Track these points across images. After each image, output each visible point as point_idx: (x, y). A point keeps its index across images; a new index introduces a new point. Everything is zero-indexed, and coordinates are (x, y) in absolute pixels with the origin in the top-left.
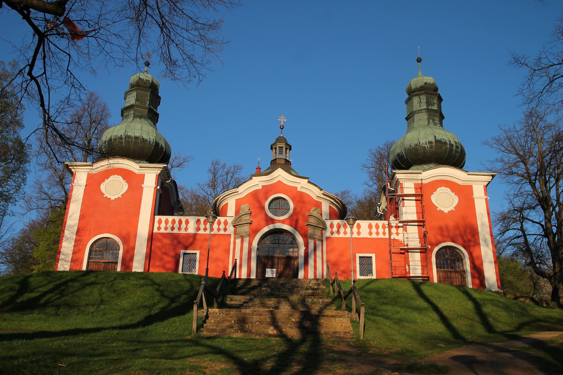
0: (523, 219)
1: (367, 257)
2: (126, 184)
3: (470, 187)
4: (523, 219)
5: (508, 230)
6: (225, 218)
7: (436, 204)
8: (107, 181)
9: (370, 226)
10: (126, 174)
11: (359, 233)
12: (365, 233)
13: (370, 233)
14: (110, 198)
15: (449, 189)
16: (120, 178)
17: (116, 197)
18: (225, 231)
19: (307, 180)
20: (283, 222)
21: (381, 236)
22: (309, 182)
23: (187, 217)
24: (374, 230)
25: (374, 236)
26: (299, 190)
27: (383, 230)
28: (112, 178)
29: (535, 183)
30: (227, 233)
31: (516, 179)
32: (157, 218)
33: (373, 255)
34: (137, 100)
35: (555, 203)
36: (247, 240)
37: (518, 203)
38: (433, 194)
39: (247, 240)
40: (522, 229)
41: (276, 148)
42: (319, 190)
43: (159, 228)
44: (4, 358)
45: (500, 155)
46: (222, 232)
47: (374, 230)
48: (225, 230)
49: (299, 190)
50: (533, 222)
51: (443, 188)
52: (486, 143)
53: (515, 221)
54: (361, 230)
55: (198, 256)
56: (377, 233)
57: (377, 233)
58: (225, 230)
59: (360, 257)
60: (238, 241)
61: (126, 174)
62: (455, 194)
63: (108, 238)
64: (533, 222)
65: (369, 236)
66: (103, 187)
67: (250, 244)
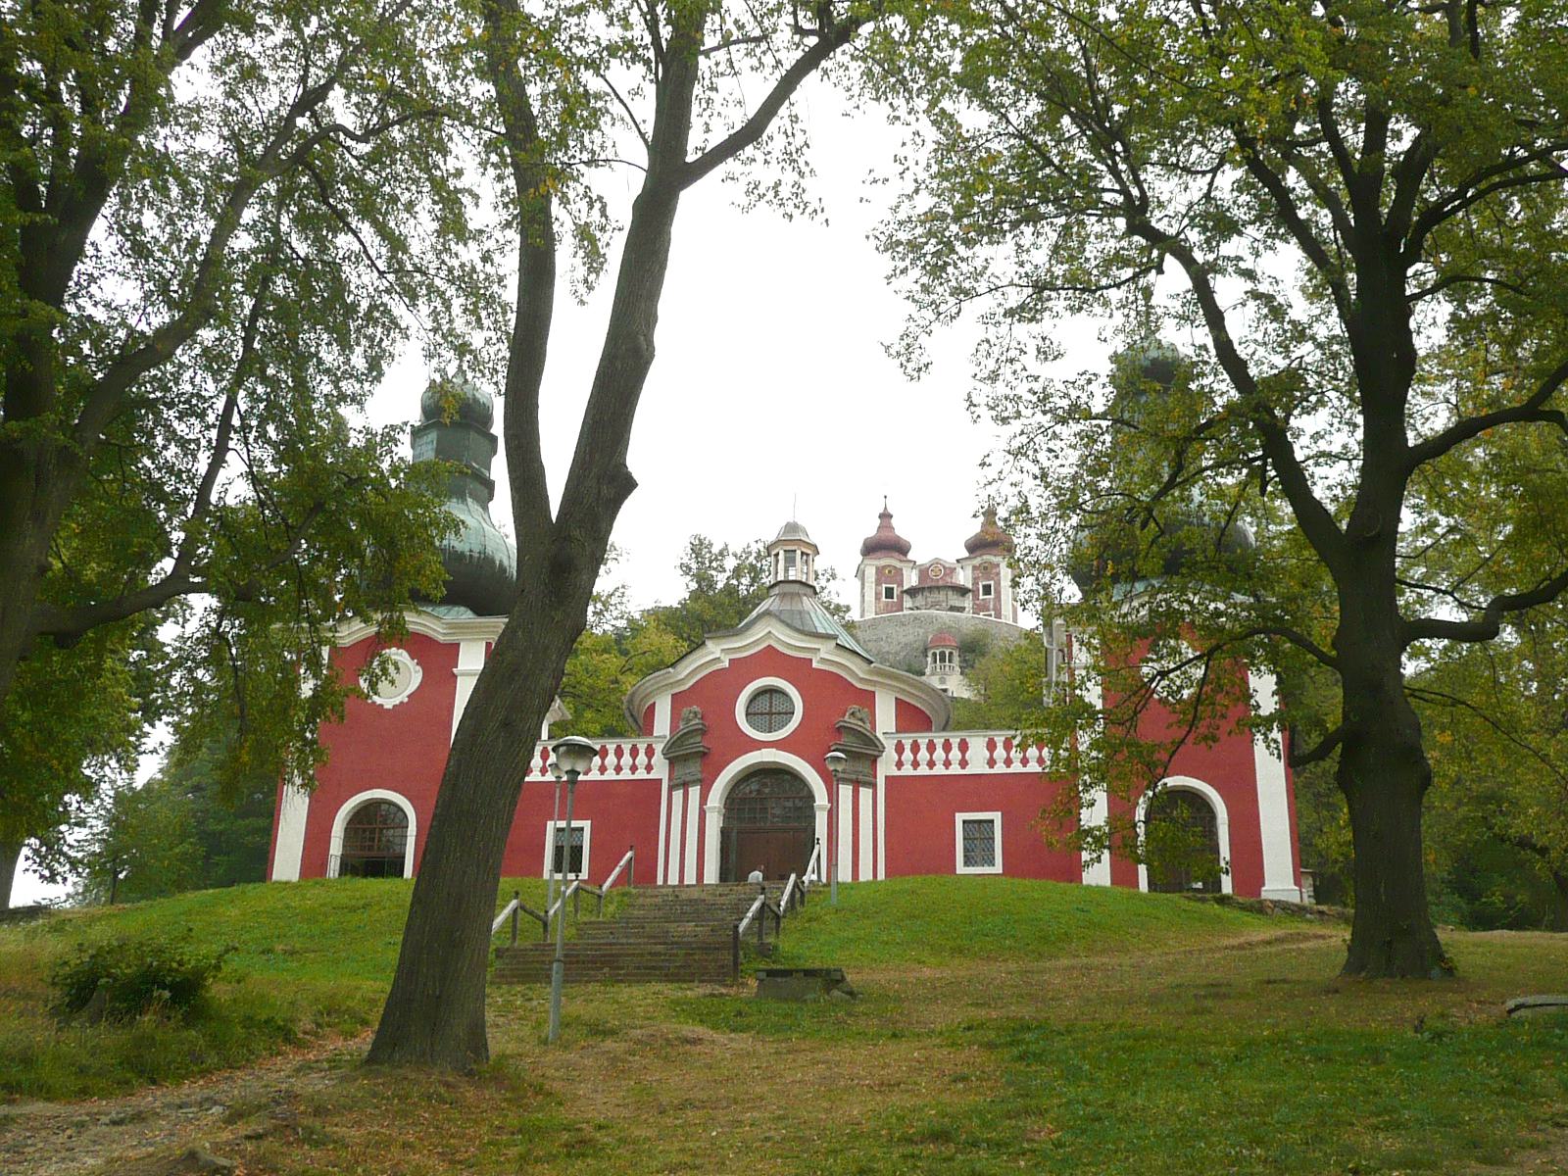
2: (418, 668)
6: (649, 740)
9: (991, 746)
11: (964, 763)
12: (978, 765)
13: (992, 763)
18: (963, 768)
19: (833, 643)
20: (777, 745)
23: (963, 734)
25: (1000, 768)
26: (815, 665)
27: (960, 756)
30: (652, 776)
33: (996, 816)
34: (438, 452)
36: (695, 792)
39: (695, 792)
41: (777, 555)
42: (865, 665)
44: (504, 38)
48: (649, 768)
49: (815, 665)
54: (968, 755)
55: (562, 824)
59: (964, 822)
60: (678, 795)
63: (401, 810)
65: (987, 770)
67: (703, 799)
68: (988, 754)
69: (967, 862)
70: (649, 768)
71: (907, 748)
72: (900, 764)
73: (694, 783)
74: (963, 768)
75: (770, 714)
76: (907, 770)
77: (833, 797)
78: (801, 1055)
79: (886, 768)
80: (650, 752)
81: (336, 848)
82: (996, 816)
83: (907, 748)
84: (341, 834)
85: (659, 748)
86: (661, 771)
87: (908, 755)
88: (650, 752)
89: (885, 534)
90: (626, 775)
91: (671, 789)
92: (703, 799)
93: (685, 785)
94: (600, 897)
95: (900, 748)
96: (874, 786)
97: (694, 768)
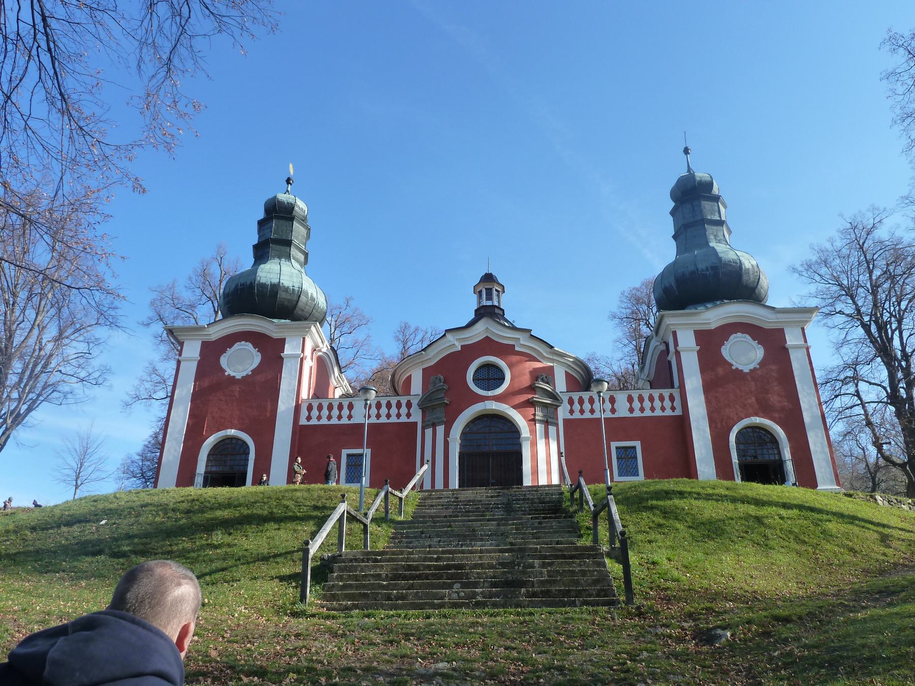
0: (856, 379)
1: (629, 447)
3: (781, 332)
4: (856, 379)
5: (836, 396)
7: (730, 360)
8: (230, 351)
10: (257, 339)
13: (631, 410)
14: (234, 377)
15: (748, 337)
16: (249, 346)
17: (244, 374)
18: (613, 413)
20: (497, 399)
21: (658, 413)
22: (552, 347)
24: (636, 404)
25: (637, 414)
28: (237, 346)
29: (870, 326)
30: (412, 420)
31: (842, 318)
32: (678, 412)
33: (637, 444)
35: (899, 354)
36: (440, 429)
37: (849, 357)
38: (723, 344)
39: (440, 429)
40: (858, 394)
42: (549, 350)
43: (309, 418)
45: (813, 288)
46: (587, 415)
47: (636, 404)
50: (870, 383)
51: (739, 334)
52: (794, 270)
53: (845, 382)
56: (653, 409)
57: (642, 410)
58: (409, 415)
60: (429, 432)
61: (257, 339)
62: (759, 343)
64: (870, 383)
65: (628, 415)
66: (224, 361)
67: (447, 434)
68: (569, 407)
69: (349, 456)
70: (409, 415)
71: (404, 405)
72: (572, 412)
73: (440, 424)
74: (613, 413)
75: (489, 379)
76: (577, 415)
77: (533, 432)
78: (88, 526)
79: (563, 413)
80: (409, 405)
81: (201, 467)
82: (637, 444)
83: (404, 405)
84: (205, 458)
85: (415, 402)
86: (417, 417)
87: (577, 406)
88: (409, 405)
89: (698, 259)
90: (394, 419)
91: (423, 429)
92: (447, 434)
93: (434, 426)
94: (401, 499)
95: (571, 402)
96: (557, 425)
97: (440, 414)
